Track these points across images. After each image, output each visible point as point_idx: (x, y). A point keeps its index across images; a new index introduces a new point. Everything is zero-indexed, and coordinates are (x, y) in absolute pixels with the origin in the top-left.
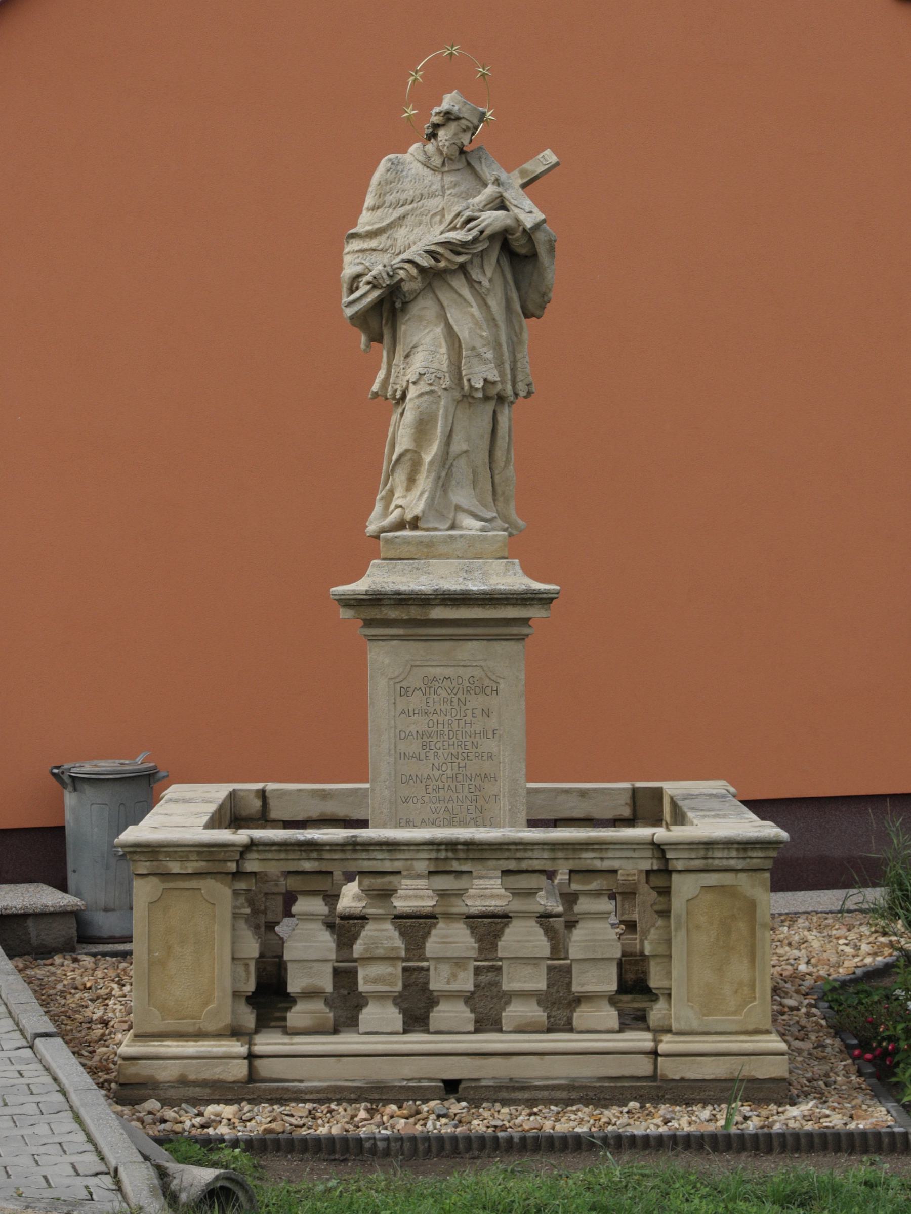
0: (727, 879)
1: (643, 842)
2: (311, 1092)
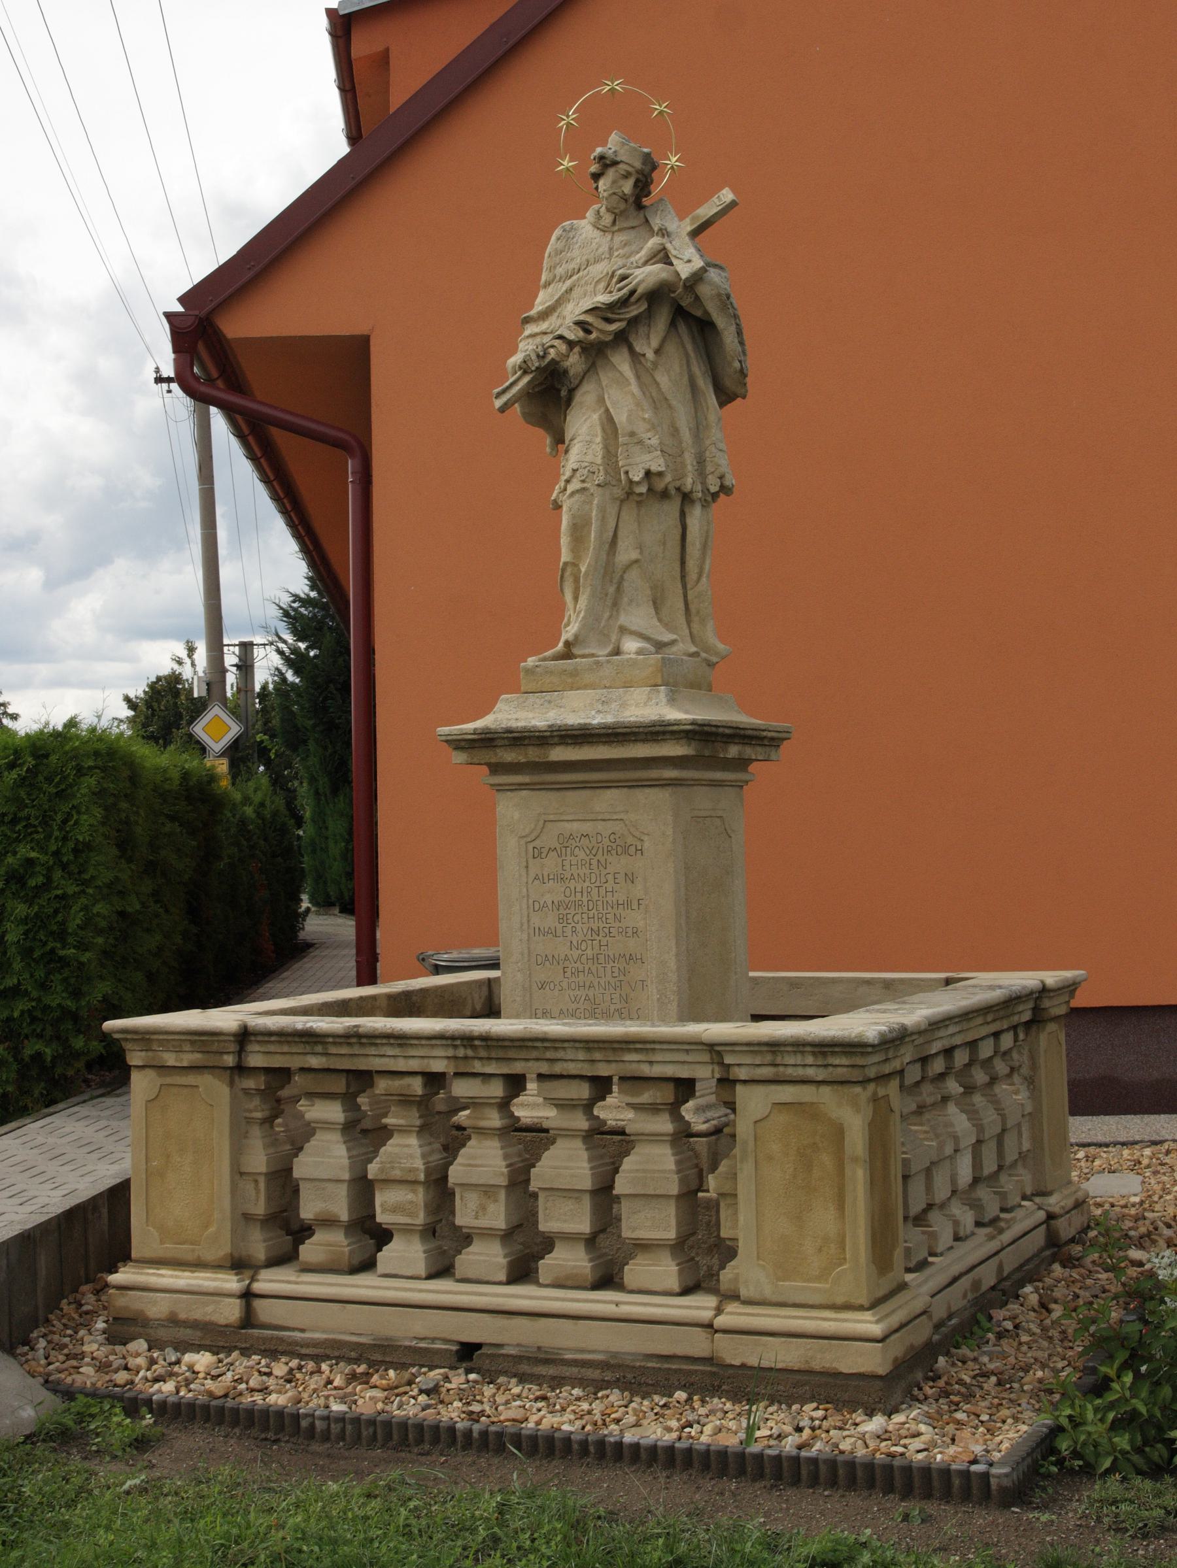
0: (805, 1094)
1: (693, 1041)
2: (307, 1345)
